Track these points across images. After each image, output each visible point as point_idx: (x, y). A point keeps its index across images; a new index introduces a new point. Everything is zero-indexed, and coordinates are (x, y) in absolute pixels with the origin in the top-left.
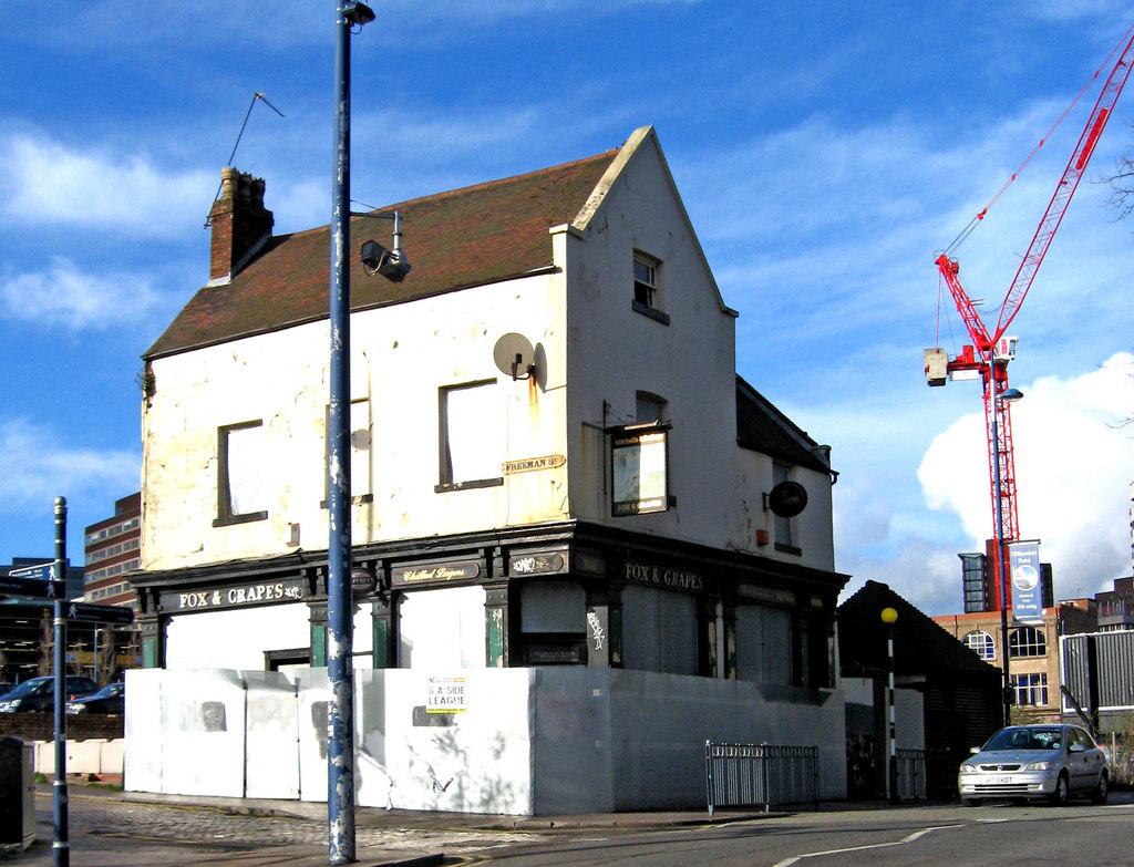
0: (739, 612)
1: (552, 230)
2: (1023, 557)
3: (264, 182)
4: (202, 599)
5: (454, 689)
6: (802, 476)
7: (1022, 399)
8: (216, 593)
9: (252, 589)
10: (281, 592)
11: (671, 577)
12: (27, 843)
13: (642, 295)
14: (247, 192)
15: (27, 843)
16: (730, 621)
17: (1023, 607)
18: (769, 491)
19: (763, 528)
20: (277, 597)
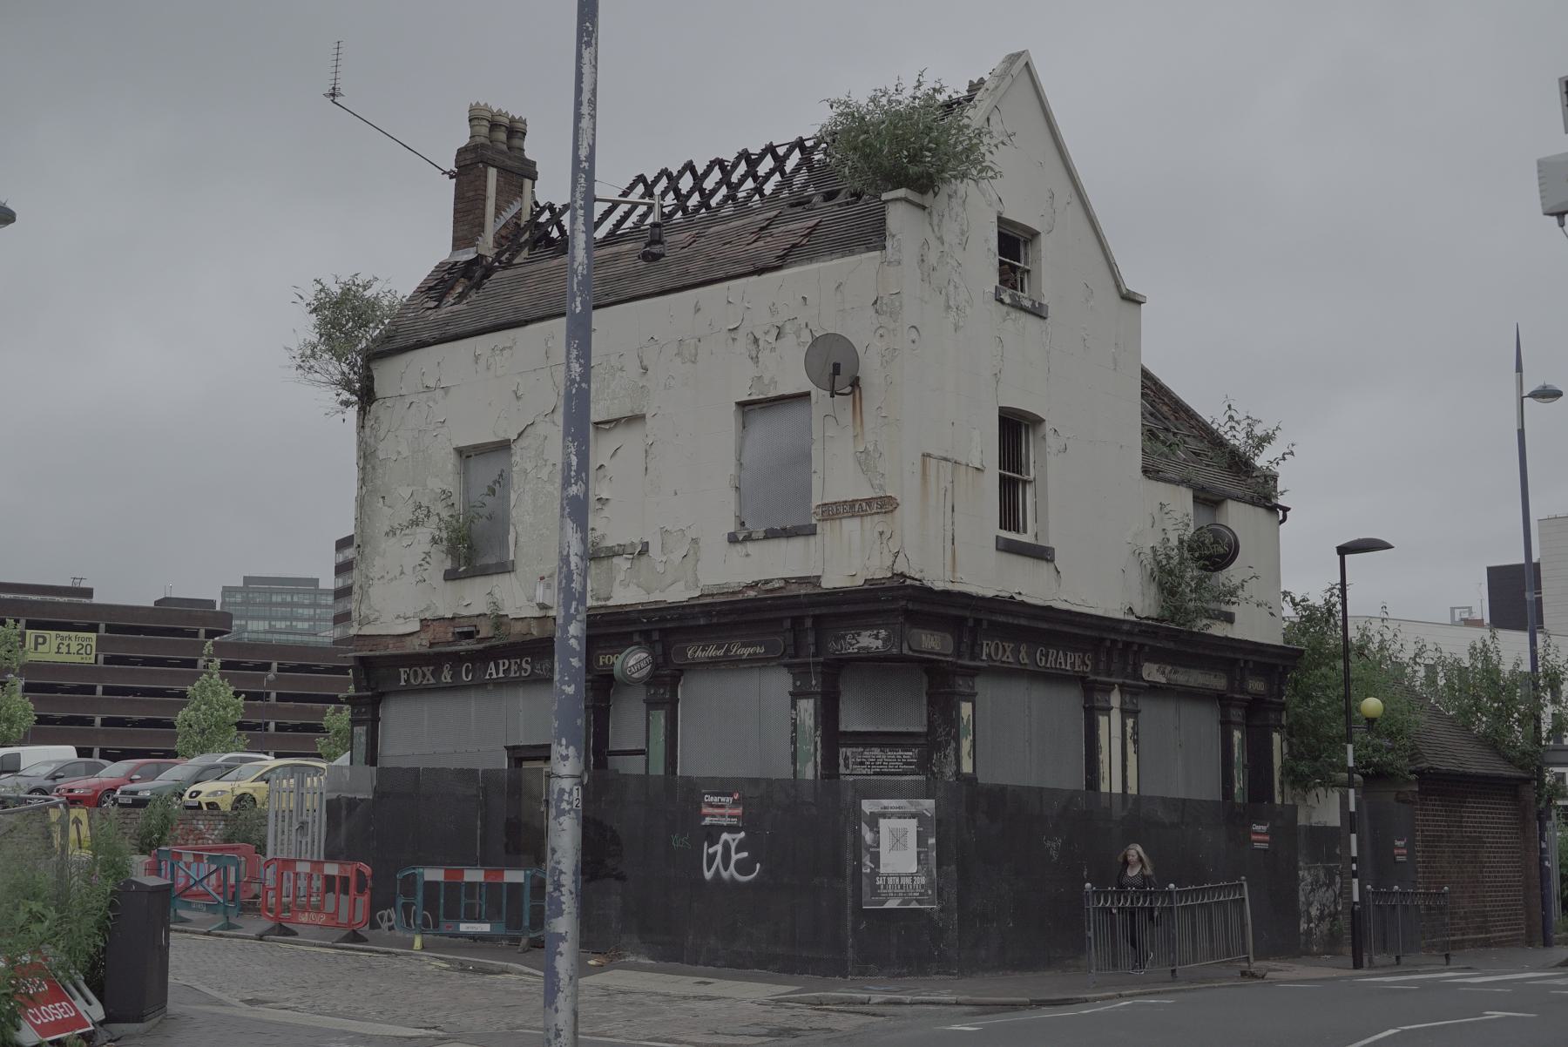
4: (429, 675)
6: (1238, 517)
10: (529, 667)
11: (1047, 656)
14: (502, 136)
20: (523, 674)
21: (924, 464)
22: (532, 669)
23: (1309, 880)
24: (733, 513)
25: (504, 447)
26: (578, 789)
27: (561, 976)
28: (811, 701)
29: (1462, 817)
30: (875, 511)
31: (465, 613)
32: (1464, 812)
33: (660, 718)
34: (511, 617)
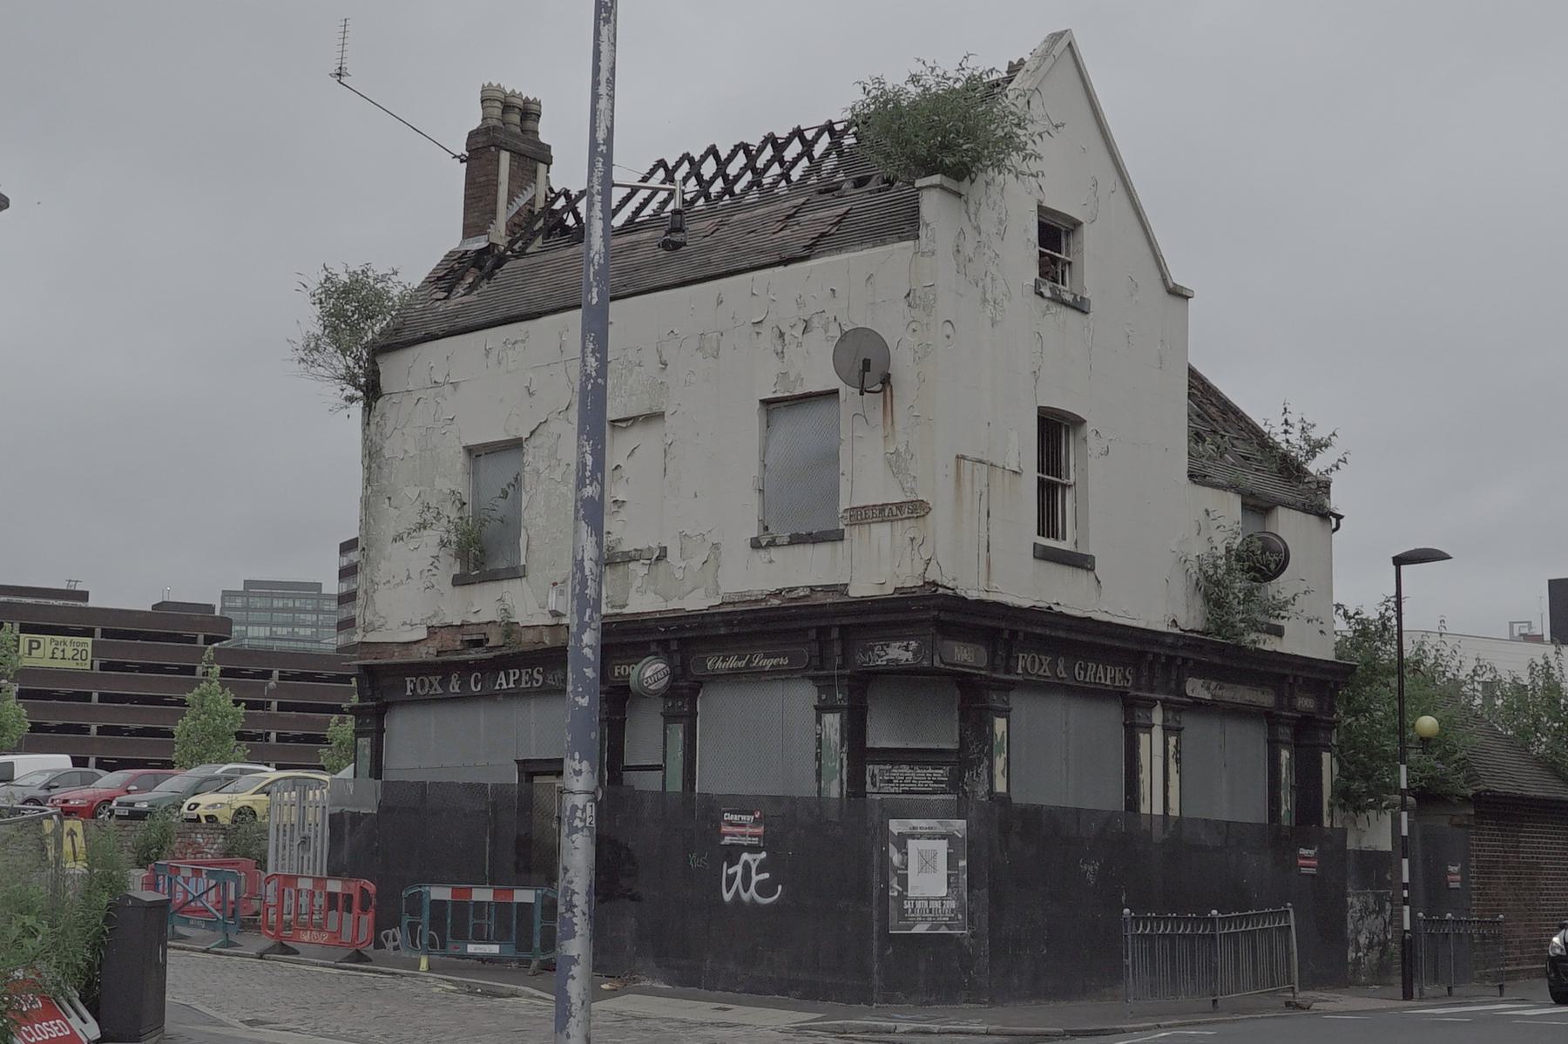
2: (1111, 673)
3: (539, 104)
9: (502, 674)
14: (515, 118)
23: (1358, 908)
29: (1520, 842)
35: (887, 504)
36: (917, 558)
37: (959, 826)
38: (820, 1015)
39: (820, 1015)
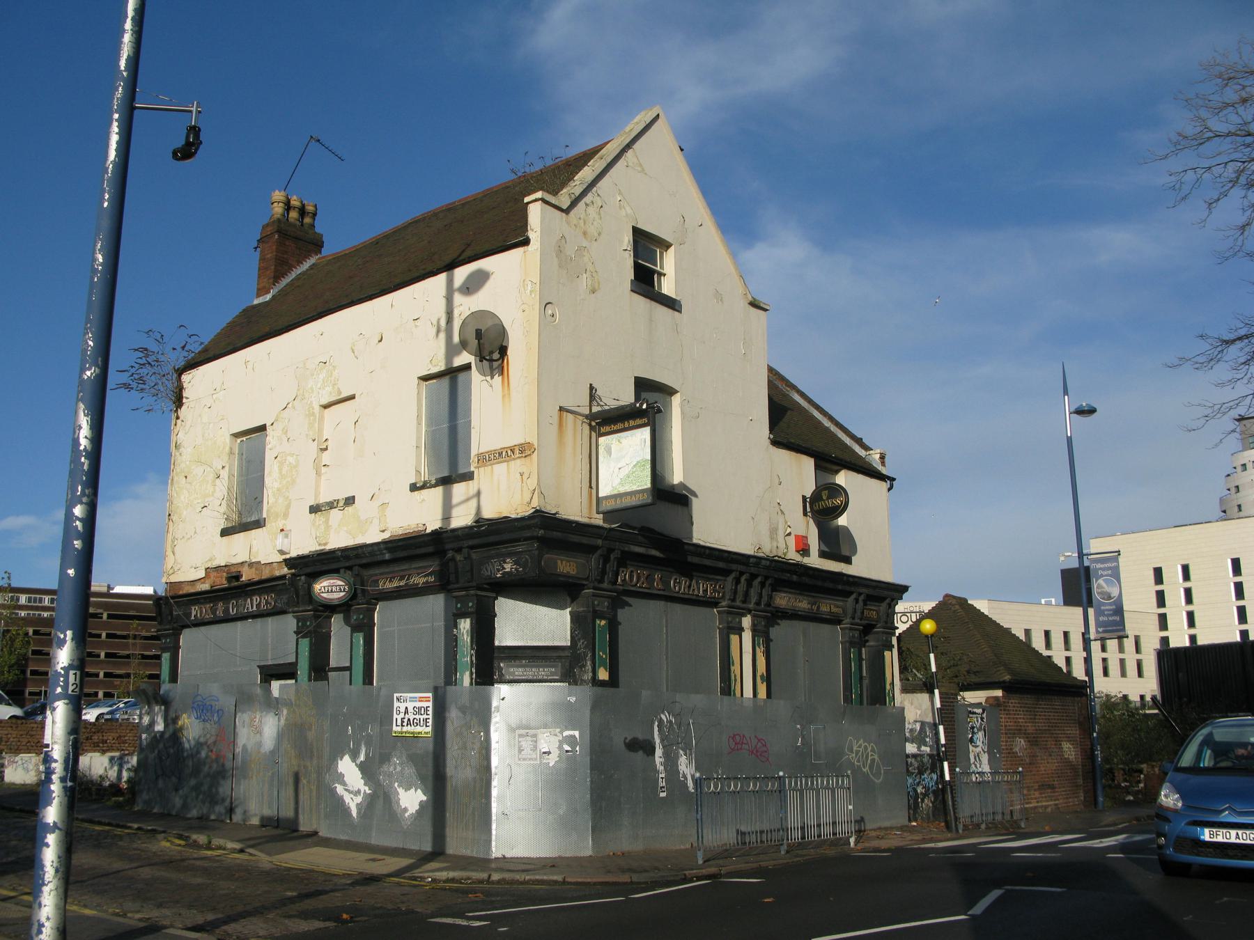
0: (780, 631)
1: (526, 200)
5: (420, 709)
7: (1095, 414)
8: (220, 604)
11: (680, 583)
12: (1087, 679)
13: (645, 280)
15: (1087, 679)
16: (760, 633)
17: (1105, 619)
18: (808, 495)
19: (802, 532)
21: (561, 418)
22: (275, 603)
23: (916, 766)
24: (414, 468)
25: (262, 428)
26: (75, 674)
27: (46, 870)
28: (468, 621)
29: (1036, 715)
30: (518, 456)
31: (234, 561)
32: (1037, 712)
33: (360, 639)
34: (262, 563)
35: (504, 448)
36: (525, 489)
37: (1206, 748)
38: (445, 865)
39: (445, 865)
